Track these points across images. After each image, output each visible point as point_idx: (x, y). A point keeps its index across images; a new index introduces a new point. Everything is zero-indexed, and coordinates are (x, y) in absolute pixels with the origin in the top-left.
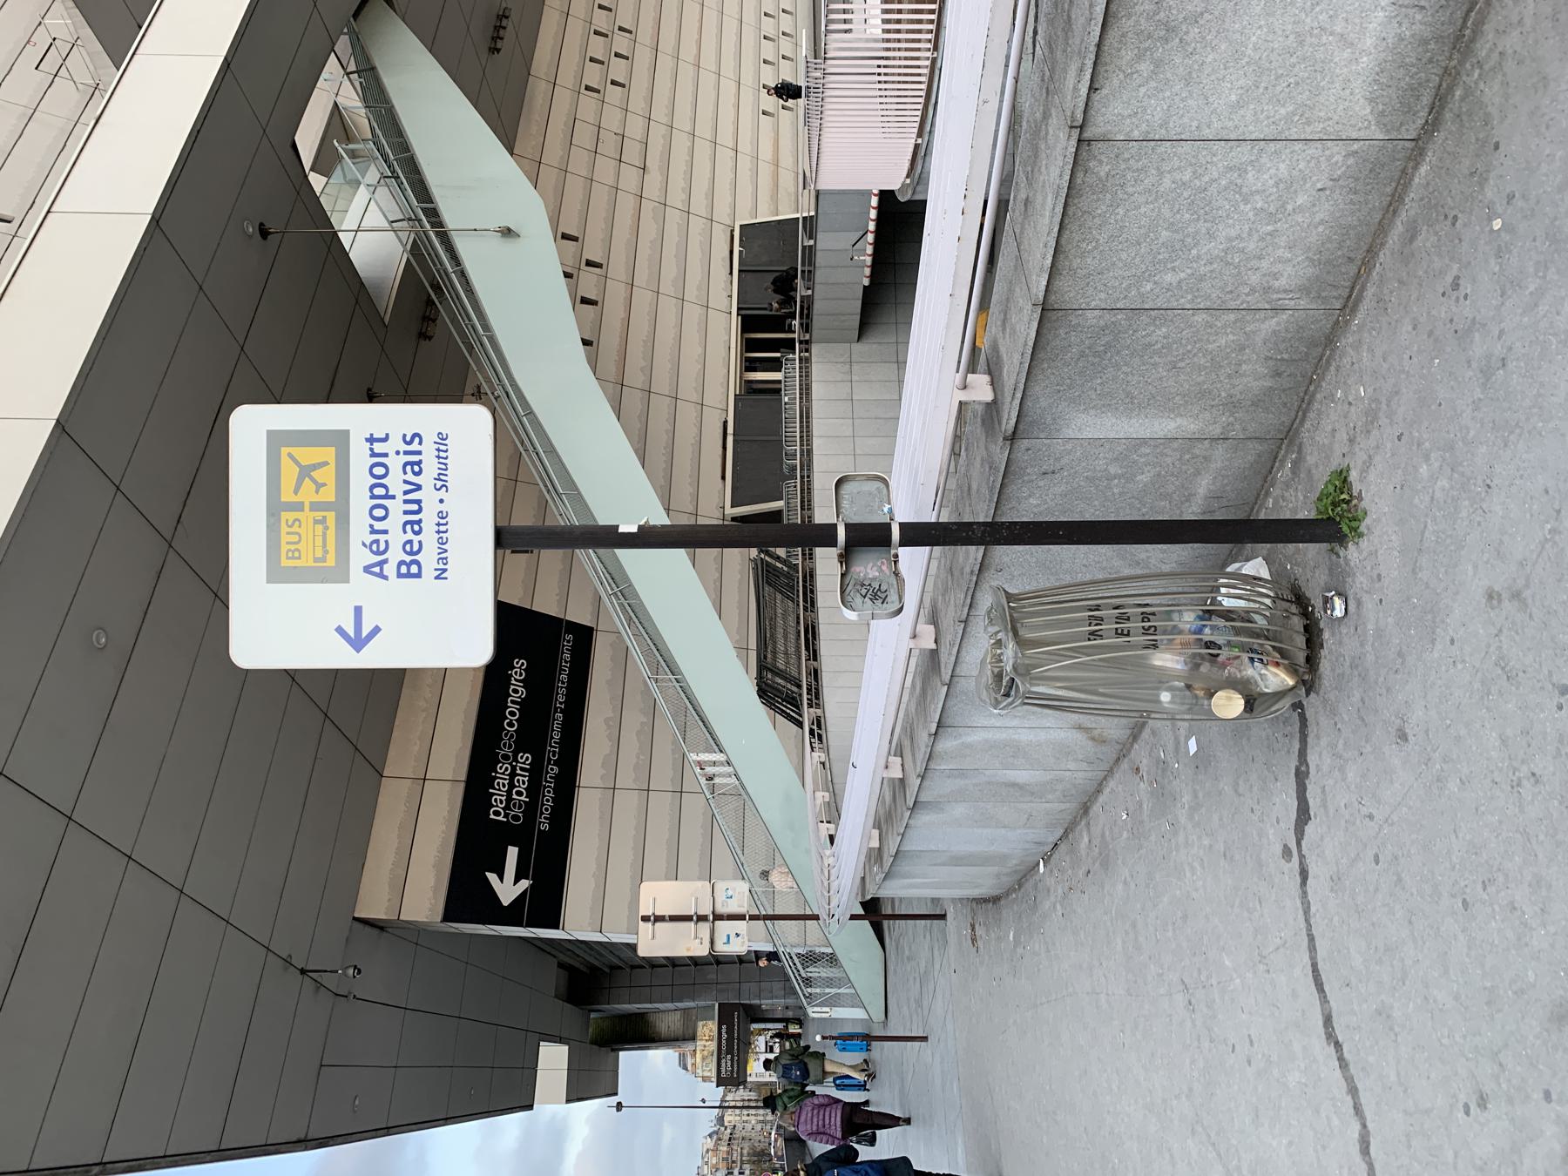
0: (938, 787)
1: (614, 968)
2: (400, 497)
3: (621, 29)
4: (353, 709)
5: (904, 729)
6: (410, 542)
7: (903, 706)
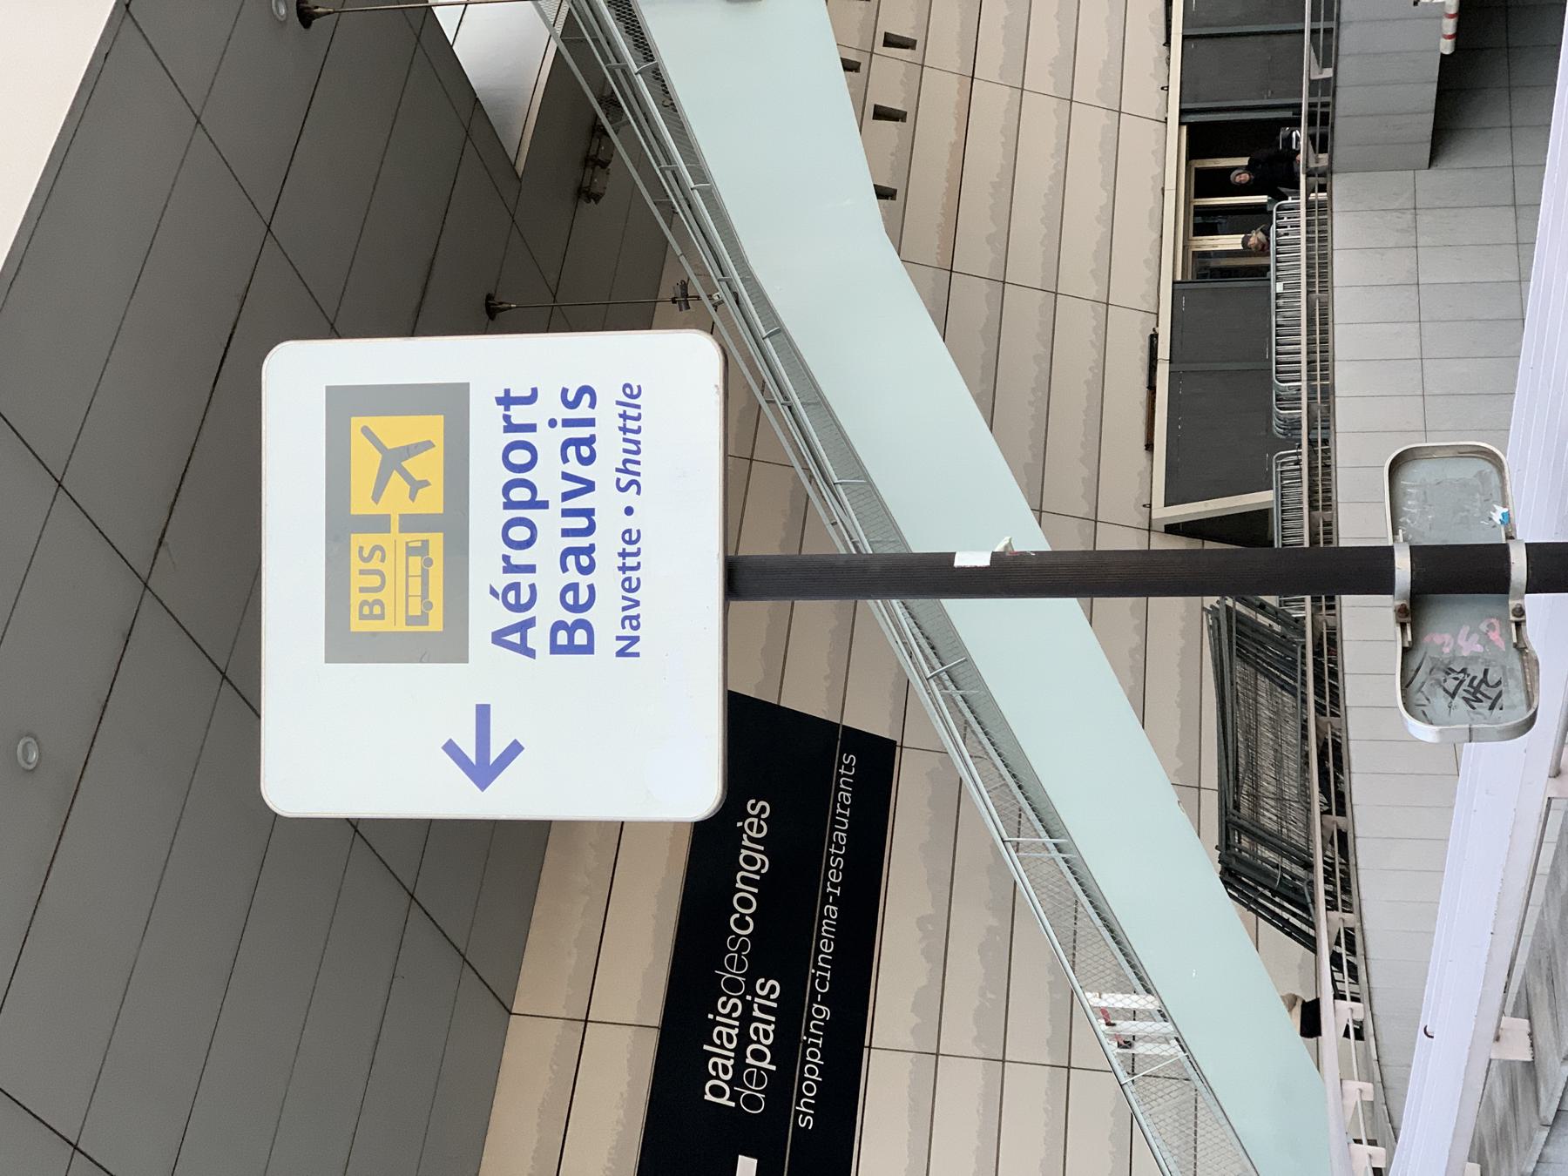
2: (557, 505)
4: (464, 888)
5: (1534, 962)
6: (574, 587)
7: (1534, 912)
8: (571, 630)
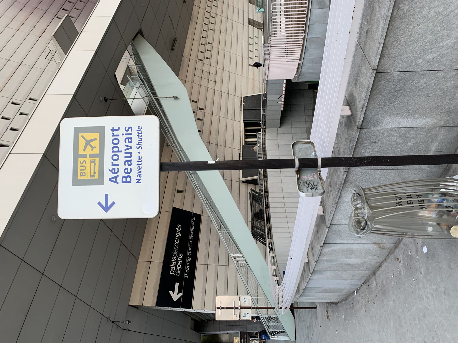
0: (322, 265)
1: (208, 320)
2: (124, 151)
3: (209, 43)
6: (127, 169)
8: (126, 178)
